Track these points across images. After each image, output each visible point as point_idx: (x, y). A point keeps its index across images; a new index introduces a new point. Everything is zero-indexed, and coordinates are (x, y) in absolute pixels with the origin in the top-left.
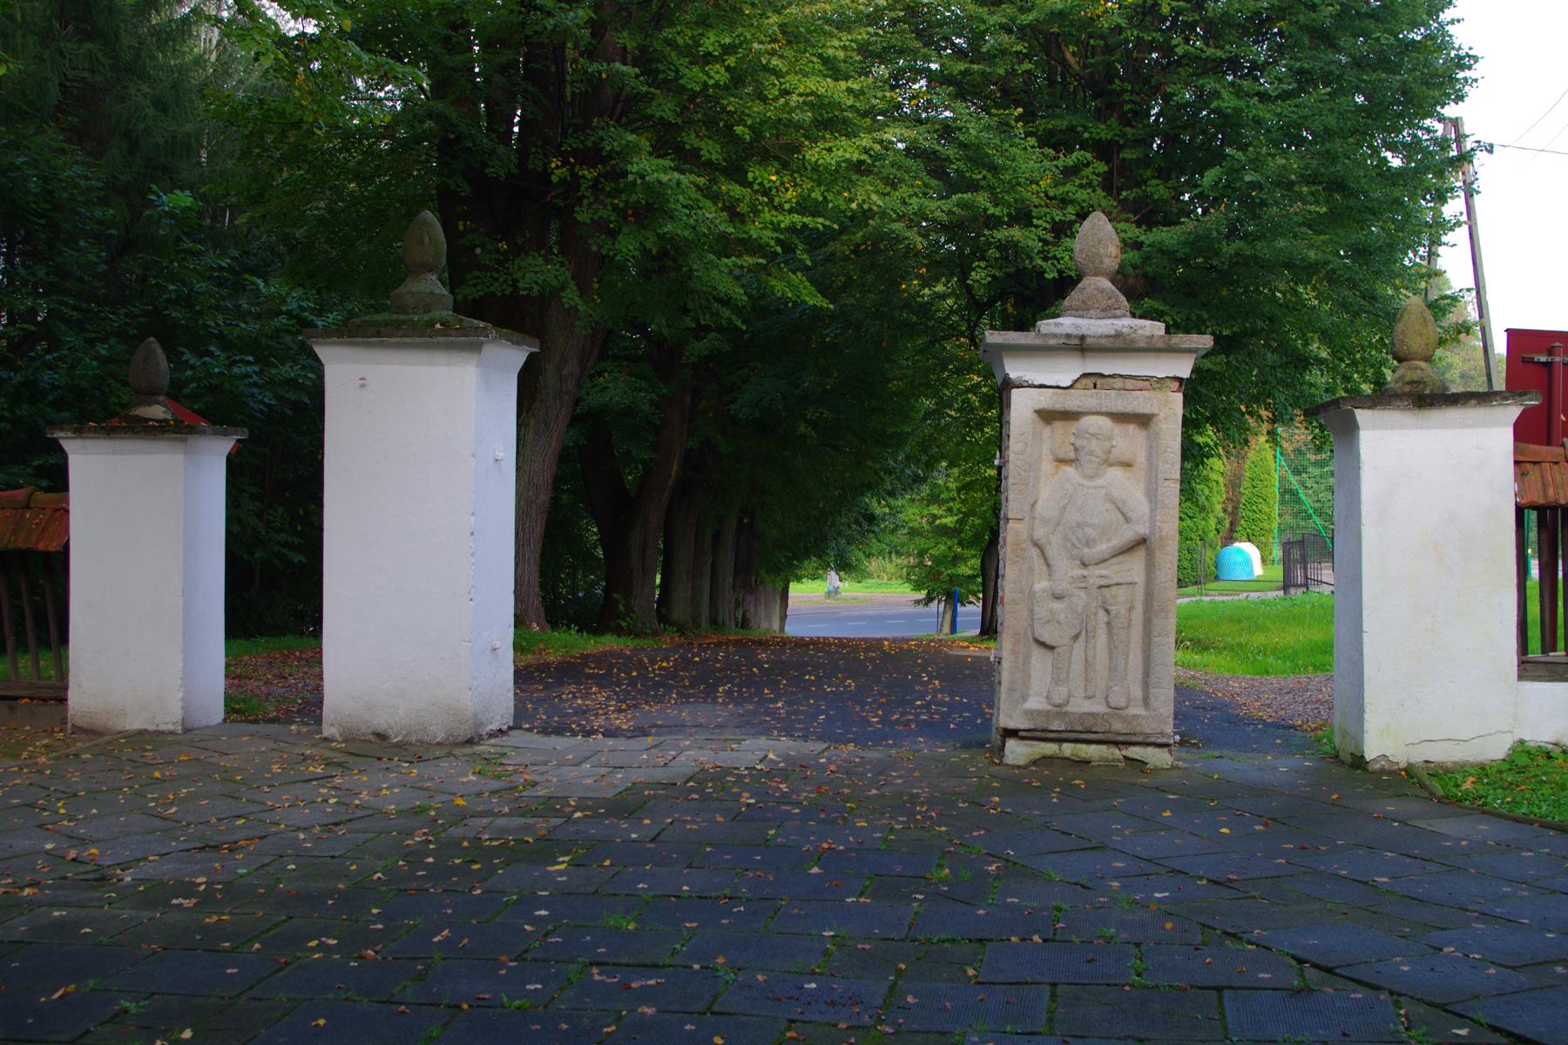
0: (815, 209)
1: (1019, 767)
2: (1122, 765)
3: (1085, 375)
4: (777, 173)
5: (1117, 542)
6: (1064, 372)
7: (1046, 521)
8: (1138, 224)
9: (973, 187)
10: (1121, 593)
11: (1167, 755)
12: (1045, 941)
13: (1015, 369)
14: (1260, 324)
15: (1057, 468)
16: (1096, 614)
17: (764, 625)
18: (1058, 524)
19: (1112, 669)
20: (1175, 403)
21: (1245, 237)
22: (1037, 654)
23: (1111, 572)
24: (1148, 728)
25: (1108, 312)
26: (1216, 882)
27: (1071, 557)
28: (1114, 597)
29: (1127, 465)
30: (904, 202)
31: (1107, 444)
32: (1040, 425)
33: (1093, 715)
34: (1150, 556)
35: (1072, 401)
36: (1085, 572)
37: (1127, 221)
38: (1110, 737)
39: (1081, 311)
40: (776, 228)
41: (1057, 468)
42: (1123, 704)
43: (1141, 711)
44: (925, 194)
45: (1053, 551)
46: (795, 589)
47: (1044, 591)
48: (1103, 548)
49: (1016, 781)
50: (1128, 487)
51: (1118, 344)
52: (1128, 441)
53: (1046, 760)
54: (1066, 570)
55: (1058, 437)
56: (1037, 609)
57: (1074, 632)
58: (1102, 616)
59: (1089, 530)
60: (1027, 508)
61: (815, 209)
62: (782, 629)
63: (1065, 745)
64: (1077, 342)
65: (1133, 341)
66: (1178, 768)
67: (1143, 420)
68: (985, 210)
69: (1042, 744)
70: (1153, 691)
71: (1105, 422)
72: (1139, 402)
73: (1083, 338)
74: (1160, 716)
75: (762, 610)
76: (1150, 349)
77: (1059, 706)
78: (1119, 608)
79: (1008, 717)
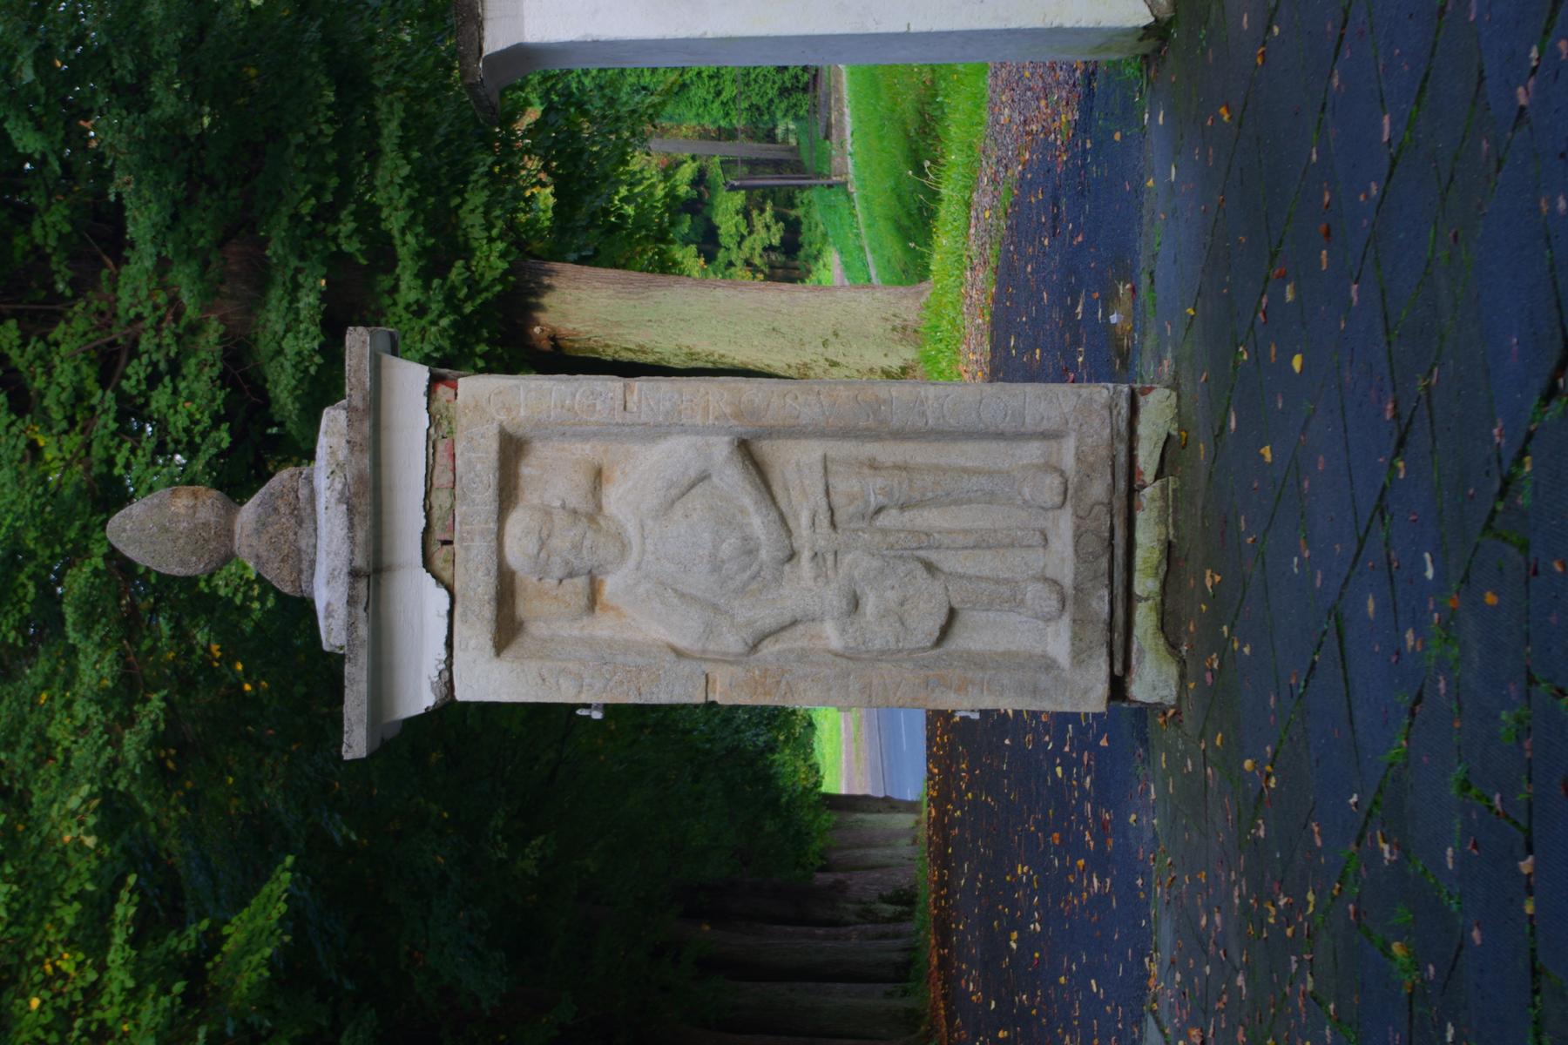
0: (98, 911)
1: (1182, 677)
2: (1172, 483)
3: (427, 563)
4: (25, 996)
5: (746, 496)
6: (420, 604)
7: (709, 630)
8: (121, 261)
9: (49, 599)
10: (844, 485)
11: (1152, 398)
12: (1530, 850)
13: (417, 697)
14: (313, 31)
15: (606, 608)
16: (885, 532)
17: (904, 848)
18: (715, 607)
19: (991, 498)
20: (475, 388)
21: (143, 75)
22: (965, 640)
23: (804, 506)
24: (1099, 432)
25: (302, 514)
26: (1401, 443)
27: (778, 580)
28: (852, 499)
29: (598, 476)
30: (84, 728)
31: (560, 519)
32: (525, 642)
33: (1078, 537)
34: (772, 433)
35: (477, 584)
36: (806, 555)
37: (114, 280)
38: (1119, 504)
39: (302, 562)
40: (133, 995)
41: (606, 608)
42: (1056, 481)
43: (1070, 444)
44: (67, 685)
45: (766, 617)
46: (834, 783)
47: (843, 631)
48: (758, 523)
49: (1214, 694)
50: (639, 477)
51: (365, 506)
52: (551, 478)
53: (1168, 627)
54: (802, 589)
55: (546, 614)
56: (878, 644)
57: (920, 572)
58: (889, 519)
59: (726, 549)
60: (685, 667)
61: (98, 911)
62: (912, 807)
63: (1139, 589)
64: (362, 585)
65: (360, 479)
66: (1176, 375)
67: (512, 449)
68: (96, 572)
69: (1138, 632)
70: (1030, 424)
71: (517, 522)
72: (477, 459)
73: (354, 574)
74: (1074, 410)
75: (877, 855)
76: (374, 412)
77: (1063, 601)
78: (874, 488)
79: (1094, 700)
